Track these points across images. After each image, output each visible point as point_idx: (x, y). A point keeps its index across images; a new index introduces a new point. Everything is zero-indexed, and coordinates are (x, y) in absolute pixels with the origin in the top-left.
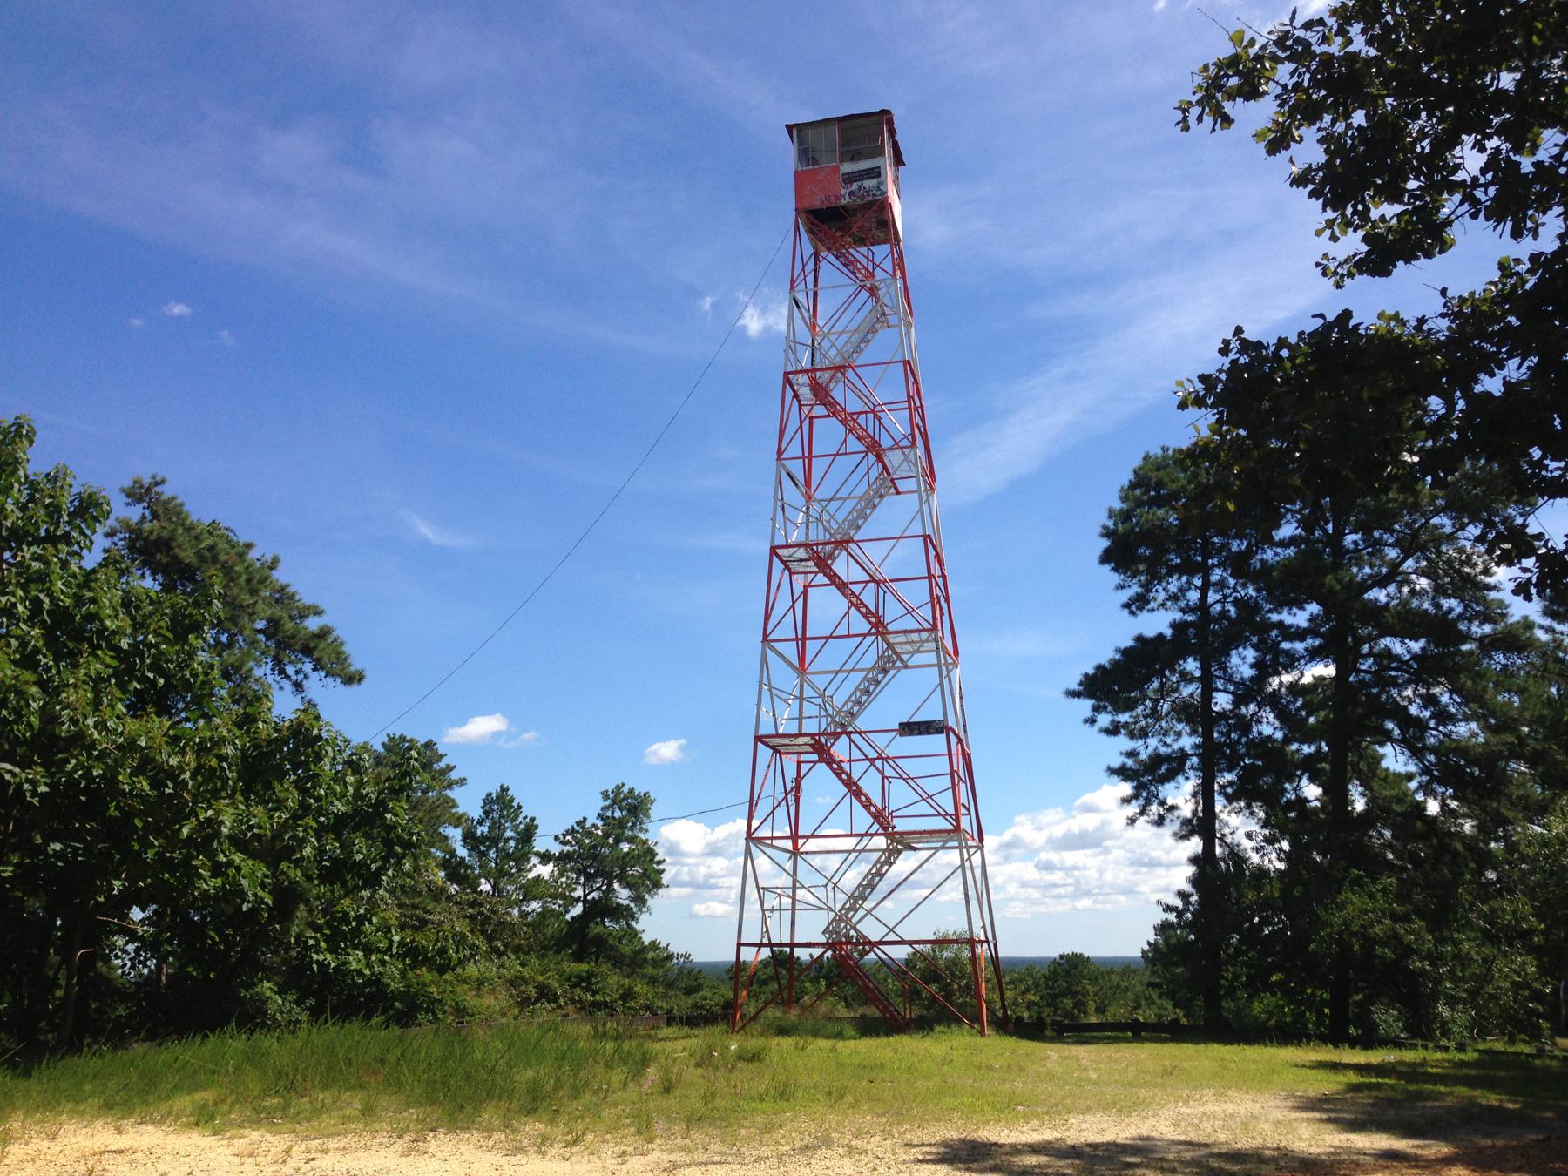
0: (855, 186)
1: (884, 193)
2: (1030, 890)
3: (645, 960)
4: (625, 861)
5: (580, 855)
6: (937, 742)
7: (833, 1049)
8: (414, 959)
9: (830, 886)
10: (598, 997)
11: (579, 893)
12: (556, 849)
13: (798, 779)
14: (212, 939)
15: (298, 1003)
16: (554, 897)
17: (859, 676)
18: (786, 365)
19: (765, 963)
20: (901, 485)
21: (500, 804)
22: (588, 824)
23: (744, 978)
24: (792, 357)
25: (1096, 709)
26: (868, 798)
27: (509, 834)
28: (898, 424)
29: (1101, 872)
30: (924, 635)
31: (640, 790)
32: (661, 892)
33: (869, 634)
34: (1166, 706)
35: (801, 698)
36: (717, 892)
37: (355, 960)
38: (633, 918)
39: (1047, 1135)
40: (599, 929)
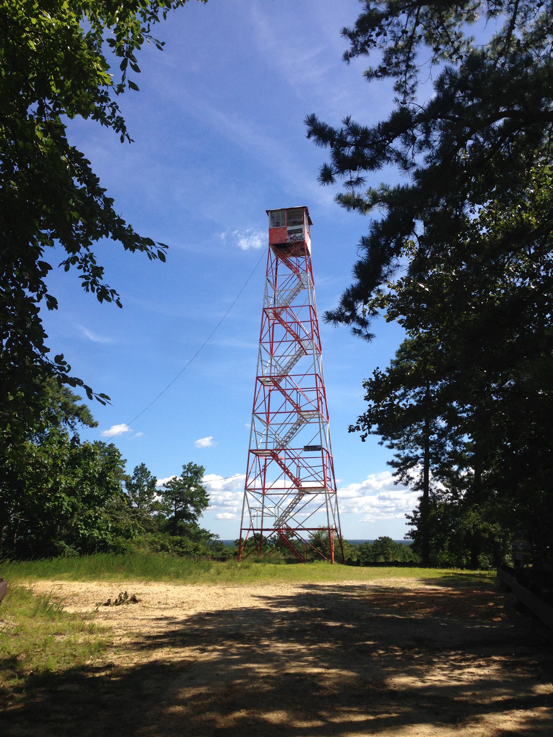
0: (292, 236)
1: (304, 239)
2: (375, 509)
3: (201, 536)
4: (193, 495)
5: (174, 492)
6: (318, 453)
7: (275, 567)
8: (117, 533)
9: (277, 507)
10: (184, 550)
11: (173, 508)
12: (164, 489)
13: (265, 466)
14: (40, 524)
15: (75, 549)
16: (163, 510)
17: (291, 426)
18: (264, 305)
19: (251, 539)
20: (308, 352)
21: (142, 471)
22: (178, 479)
23: (242, 544)
24: (266, 301)
25: (384, 439)
26: (292, 474)
27: (145, 483)
28: (307, 328)
29: (408, 501)
30: (315, 413)
31: (199, 465)
32: (207, 508)
33: (293, 412)
34: (412, 438)
35: (267, 435)
36: (227, 508)
37: (96, 533)
38: (196, 519)
39: (335, 584)
40: (181, 523)
